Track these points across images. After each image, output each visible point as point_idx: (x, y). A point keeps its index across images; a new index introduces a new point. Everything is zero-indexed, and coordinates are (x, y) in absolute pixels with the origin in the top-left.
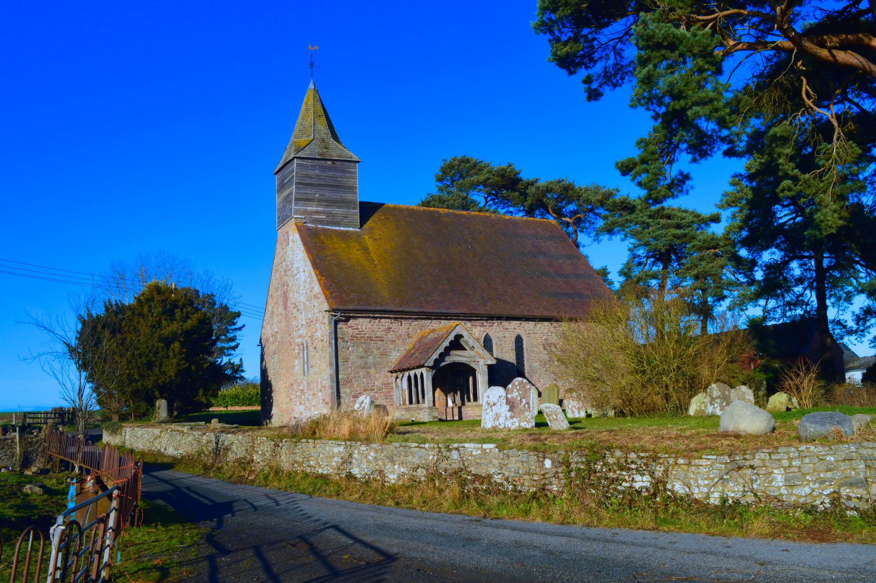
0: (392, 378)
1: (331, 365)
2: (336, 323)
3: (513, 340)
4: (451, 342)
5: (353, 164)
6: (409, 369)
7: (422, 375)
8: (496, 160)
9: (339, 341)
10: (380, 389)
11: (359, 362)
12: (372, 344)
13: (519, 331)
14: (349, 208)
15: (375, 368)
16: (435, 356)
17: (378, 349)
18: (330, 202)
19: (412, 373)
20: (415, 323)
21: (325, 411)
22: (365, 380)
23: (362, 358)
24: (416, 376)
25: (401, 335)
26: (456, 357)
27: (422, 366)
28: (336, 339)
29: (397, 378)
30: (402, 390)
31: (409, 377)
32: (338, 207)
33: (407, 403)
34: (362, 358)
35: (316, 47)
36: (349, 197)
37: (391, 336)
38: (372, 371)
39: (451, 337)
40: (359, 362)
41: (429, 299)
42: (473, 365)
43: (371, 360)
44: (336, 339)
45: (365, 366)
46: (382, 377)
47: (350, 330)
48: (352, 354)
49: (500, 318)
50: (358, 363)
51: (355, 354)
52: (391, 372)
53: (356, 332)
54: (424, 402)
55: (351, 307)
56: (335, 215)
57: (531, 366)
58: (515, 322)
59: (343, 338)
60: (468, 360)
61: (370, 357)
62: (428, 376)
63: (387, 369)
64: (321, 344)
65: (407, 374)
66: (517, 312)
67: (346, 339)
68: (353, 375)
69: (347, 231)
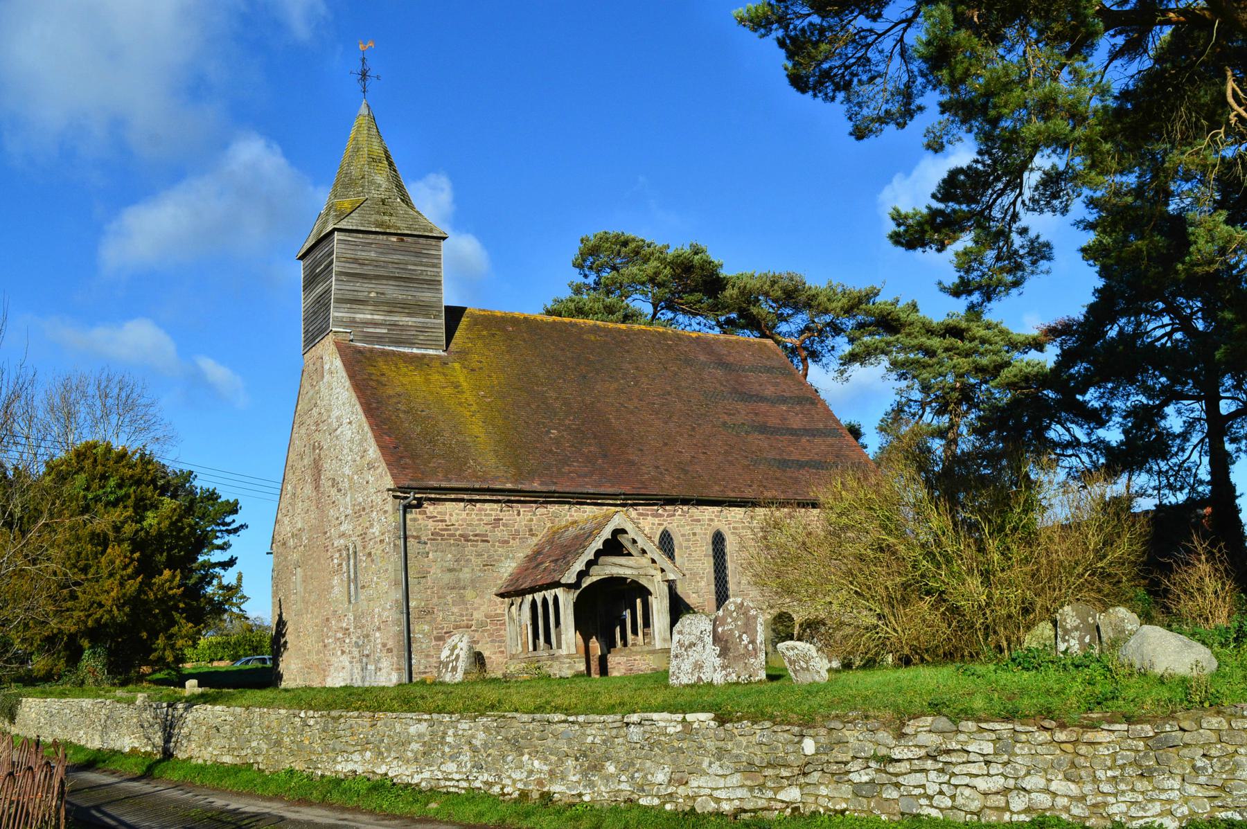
0: (501, 605)
4: (606, 542)
6: (532, 590)
7: (556, 599)
8: (668, 233)
9: (411, 542)
10: (482, 625)
11: (447, 577)
12: (469, 548)
14: (427, 316)
15: (474, 588)
16: (579, 566)
17: (479, 555)
19: (539, 597)
20: (541, 510)
22: (455, 610)
23: (450, 570)
24: (545, 601)
27: (557, 584)
28: (405, 538)
31: (534, 603)
32: (410, 315)
33: (531, 648)
34: (450, 570)
36: (426, 296)
37: (501, 533)
38: (469, 594)
39: (606, 533)
40: (447, 577)
43: (466, 575)
44: (405, 538)
45: (457, 586)
46: (487, 604)
47: (430, 523)
48: (434, 564)
49: (685, 502)
50: (446, 580)
51: (439, 565)
52: (502, 595)
53: (441, 525)
54: (559, 647)
55: (436, 484)
56: (404, 328)
58: (711, 509)
59: (417, 537)
60: (635, 572)
62: (567, 600)
63: (495, 590)
65: (529, 598)
66: (714, 492)
67: (424, 539)
69: (424, 356)
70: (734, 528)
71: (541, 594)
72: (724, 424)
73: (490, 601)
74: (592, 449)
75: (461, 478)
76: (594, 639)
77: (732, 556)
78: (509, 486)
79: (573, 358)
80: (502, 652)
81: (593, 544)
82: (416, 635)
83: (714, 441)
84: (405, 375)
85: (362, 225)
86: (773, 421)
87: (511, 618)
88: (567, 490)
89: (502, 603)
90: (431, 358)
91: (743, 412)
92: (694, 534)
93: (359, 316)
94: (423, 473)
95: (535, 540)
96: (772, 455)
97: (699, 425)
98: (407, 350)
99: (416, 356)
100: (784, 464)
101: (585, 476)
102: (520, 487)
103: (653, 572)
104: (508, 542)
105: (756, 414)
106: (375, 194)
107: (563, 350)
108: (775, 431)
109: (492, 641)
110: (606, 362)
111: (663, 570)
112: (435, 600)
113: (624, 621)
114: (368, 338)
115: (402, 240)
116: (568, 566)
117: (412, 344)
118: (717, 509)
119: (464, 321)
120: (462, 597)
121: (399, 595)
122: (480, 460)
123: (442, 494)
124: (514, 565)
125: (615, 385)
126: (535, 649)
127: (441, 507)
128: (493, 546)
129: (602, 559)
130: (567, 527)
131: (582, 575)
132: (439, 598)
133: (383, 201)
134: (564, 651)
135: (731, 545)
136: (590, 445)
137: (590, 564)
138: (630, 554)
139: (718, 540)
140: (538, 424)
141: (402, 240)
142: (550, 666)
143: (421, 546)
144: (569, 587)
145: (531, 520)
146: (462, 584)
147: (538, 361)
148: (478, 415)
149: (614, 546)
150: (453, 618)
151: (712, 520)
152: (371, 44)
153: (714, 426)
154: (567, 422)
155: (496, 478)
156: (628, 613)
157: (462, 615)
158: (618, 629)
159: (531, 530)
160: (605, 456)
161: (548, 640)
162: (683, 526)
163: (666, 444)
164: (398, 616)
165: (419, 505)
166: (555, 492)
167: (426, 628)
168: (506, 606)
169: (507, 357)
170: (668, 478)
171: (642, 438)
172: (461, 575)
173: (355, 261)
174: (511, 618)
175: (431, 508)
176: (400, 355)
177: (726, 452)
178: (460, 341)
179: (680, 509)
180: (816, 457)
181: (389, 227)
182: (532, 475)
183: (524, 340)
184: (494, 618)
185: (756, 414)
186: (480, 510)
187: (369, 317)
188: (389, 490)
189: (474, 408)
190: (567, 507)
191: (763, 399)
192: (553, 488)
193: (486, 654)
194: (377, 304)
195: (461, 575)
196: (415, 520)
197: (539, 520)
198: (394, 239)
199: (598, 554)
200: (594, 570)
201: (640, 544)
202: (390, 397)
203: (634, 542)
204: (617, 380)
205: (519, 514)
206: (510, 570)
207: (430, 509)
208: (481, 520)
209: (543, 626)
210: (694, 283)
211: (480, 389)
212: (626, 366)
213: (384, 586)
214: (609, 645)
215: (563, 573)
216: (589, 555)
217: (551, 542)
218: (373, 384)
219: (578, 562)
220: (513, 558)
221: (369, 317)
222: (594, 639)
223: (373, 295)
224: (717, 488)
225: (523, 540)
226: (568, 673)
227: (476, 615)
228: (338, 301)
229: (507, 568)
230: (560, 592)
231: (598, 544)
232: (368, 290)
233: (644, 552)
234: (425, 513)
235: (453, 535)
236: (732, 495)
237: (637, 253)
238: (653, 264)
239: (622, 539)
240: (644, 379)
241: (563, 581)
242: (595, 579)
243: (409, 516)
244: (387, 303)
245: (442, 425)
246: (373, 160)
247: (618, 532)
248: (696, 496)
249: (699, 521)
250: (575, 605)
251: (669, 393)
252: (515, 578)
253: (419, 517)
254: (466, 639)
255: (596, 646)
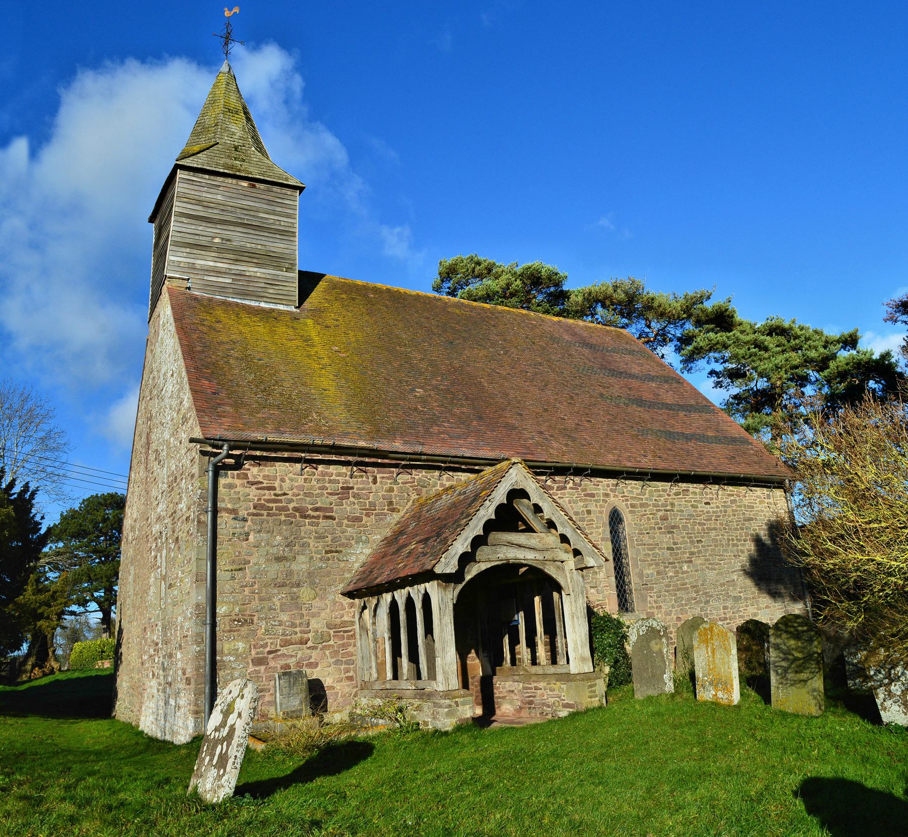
0: (349, 609)
1: (198, 579)
2: (218, 470)
3: (606, 519)
4: (500, 509)
5: (289, 192)
6: (392, 586)
7: (426, 599)
8: (512, 259)
9: (224, 519)
10: (323, 638)
11: (274, 570)
12: (307, 527)
13: (616, 501)
14: (278, 268)
15: (313, 585)
16: (461, 545)
17: (320, 537)
18: (242, 255)
19: (400, 596)
20: (404, 477)
21: (717, 404)
22: (284, 617)
23: (279, 559)
24: (410, 602)
25: (373, 504)
26: (512, 549)
27: (428, 576)
28: (215, 512)
29: (364, 608)
30: (375, 641)
31: (394, 605)
32: (258, 265)
33: (389, 675)
34: (279, 559)
35: (236, 10)
36: (278, 246)
37: (350, 507)
38: (305, 593)
39: (500, 496)
40: (274, 570)
41: (435, 429)
42: (550, 570)
43: (301, 565)
44: (215, 512)
45: (287, 583)
46: (332, 607)
47: (253, 491)
48: (251, 550)
49: (579, 471)
50: (271, 575)
51: (263, 551)
52: (350, 595)
54: (432, 676)
55: (259, 436)
56: (250, 279)
57: (641, 575)
58: (605, 481)
59: (234, 511)
60: (539, 556)
61: (301, 558)
62: (442, 600)
63: (341, 587)
64: (185, 527)
65: (387, 597)
66: (609, 461)
67: (242, 513)
68: (255, 604)
69: (273, 310)
70: (633, 506)
71: (422, 587)
72: (602, 395)
73: (334, 602)
74: (465, 410)
75: (296, 430)
76: (473, 654)
77: (631, 540)
78: (362, 444)
79: (438, 326)
80: (350, 678)
81: (482, 512)
82: (225, 656)
83: (595, 410)
84: (247, 324)
85: (208, 165)
86: (647, 396)
87: (363, 628)
88: (438, 452)
89: (352, 606)
90: (280, 313)
91: (617, 387)
92: (589, 512)
93: (200, 262)
94: (245, 424)
95: (396, 517)
96: (656, 426)
97: (577, 394)
98: (253, 303)
99: (264, 310)
100: (671, 436)
101: (459, 437)
102: (375, 445)
103: (563, 556)
104: (359, 519)
105: (630, 389)
106: (226, 140)
107: (427, 318)
108: (651, 405)
109: (337, 662)
110: (473, 332)
111: (577, 553)
112: (255, 604)
113: (517, 627)
114: (208, 286)
115: (254, 186)
116: (445, 546)
117: (259, 297)
118: (612, 481)
119: (322, 285)
120: (295, 598)
121: (202, 597)
122: (326, 414)
123: (269, 451)
124: (368, 551)
125: (484, 352)
126: (395, 677)
127: (268, 470)
128: (340, 525)
129: (494, 536)
130: (438, 496)
131: (466, 559)
132: (261, 599)
133: (236, 148)
134: (440, 685)
135: (629, 527)
136: (462, 405)
137: (478, 542)
138: (530, 529)
139: (615, 519)
140: (400, 382)
141: (254, 186)
142: (419, 708)
143: (238, 524)
144: (447, 579)
145: (391, 490)
146: (295, 579)
147: (401, 325)
148: (329, 368)
149: (508, 518)
150: (280, 630)
151: (607, 495)
152: (236, 10)
153: (591, 396)
154: (434, 382)
155: (346, 435)
156: (521, 617)
157: (293, 625)
158: (506, 639)
159: (391, 503)
160: (480, 418)
161: (414, 657)
162: (575, 502)
163: (546, 410)
164: (199, 629)
165: (238, 466)
166: (421, 454)
167: (241, 645)
168: (357, 610)
169: (367, 318)
170: (555, 445)
171: (519, 402)
172: (294, 567)
173: (199, 202)
174: (363, 628)
175: (255, 470)
176: (244, 307)
177: (610, 421)
178: (316, 301)
179: (572, 481)
180: (698, 431)
181: (239, 171)
182: (392, 433)
183: (386, 306)
184: (339, 628)
185: (630, 389)
186: (323, 474)
187: (212, 264)
188: (192, 440)
189: (326, 361)
190: (437, 473)
191: (632, 376)
192: (419, 449)
193: (327, 682)
194: (222, 251)
195: (294, 567)
196: (230, 486)
197: (401, 491)
198: (245, 184)
199: (489, 526)
200: (483, 552)
201: (547, 513)
202: (221, 343)
203: (537, 509)
204: (485, 348)
205: (375, 481)
206: (362, 558)
207: (253, 471)
208: (323, 488)
209: (407, 636)
210: (542, 290)
211: (334, 344)
212: (493, 337)
213: (188, 582)
214: (494, 660)
215: (437, 557)
216: (476, 528)
217: (417, 516)
218: (205, 329)
219: (460, 539)
220: (367, 541)
221: (212, 264)
222: (473, 654)
223: (217, 240)
224: (611, 456)
225: (381, 516)
226: (447, 724)
227: (314, 624)
228: (176, 244)
229: (360, 555)
230: (432, 588)
231: (488, 512)
232: (214, 234)
233: (551, 525)
234: (246, 476)
235: (285, 509)
236: (629, 464)
237: (489, 270)
238: (504, 277)
239: (523, 507)
240: (513, 350)
241: (438, 570)
242: (483, 566)
243: (222, 481)
244: (234, 251)
245: (283, 375)
246: (229, 110)
247: (517, 494)
248: (590, 465)
249: (592, 495)
250: (455, 606)
251: (540, 364)
252: (368, 569)
253: (238, 482)
254: (249, 692)
255: (475, 662)
